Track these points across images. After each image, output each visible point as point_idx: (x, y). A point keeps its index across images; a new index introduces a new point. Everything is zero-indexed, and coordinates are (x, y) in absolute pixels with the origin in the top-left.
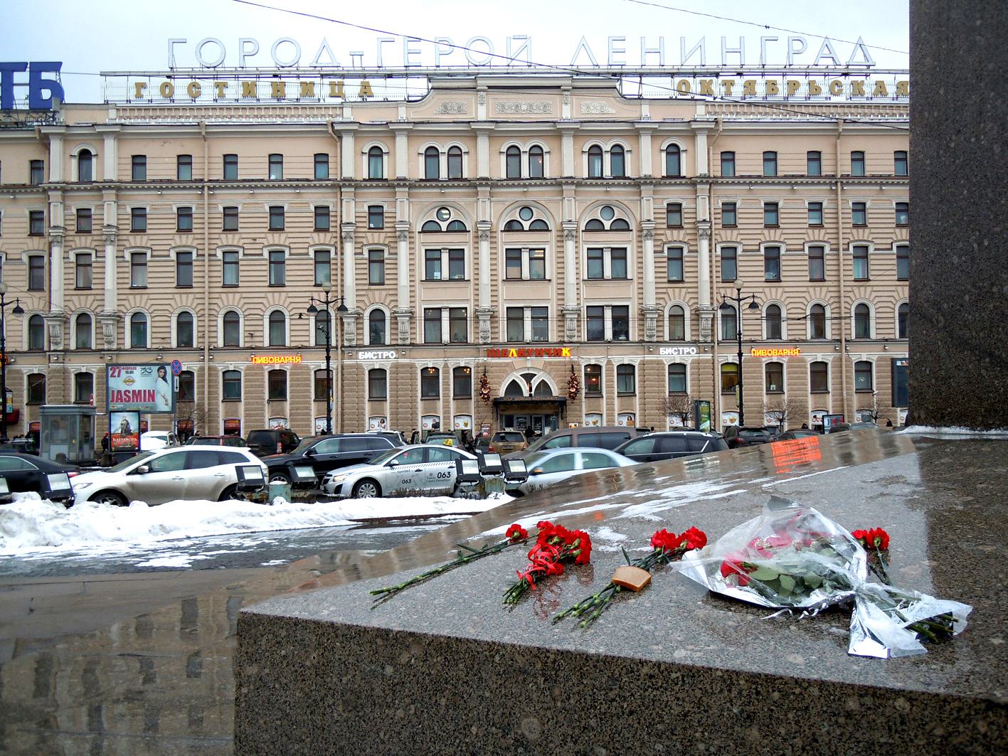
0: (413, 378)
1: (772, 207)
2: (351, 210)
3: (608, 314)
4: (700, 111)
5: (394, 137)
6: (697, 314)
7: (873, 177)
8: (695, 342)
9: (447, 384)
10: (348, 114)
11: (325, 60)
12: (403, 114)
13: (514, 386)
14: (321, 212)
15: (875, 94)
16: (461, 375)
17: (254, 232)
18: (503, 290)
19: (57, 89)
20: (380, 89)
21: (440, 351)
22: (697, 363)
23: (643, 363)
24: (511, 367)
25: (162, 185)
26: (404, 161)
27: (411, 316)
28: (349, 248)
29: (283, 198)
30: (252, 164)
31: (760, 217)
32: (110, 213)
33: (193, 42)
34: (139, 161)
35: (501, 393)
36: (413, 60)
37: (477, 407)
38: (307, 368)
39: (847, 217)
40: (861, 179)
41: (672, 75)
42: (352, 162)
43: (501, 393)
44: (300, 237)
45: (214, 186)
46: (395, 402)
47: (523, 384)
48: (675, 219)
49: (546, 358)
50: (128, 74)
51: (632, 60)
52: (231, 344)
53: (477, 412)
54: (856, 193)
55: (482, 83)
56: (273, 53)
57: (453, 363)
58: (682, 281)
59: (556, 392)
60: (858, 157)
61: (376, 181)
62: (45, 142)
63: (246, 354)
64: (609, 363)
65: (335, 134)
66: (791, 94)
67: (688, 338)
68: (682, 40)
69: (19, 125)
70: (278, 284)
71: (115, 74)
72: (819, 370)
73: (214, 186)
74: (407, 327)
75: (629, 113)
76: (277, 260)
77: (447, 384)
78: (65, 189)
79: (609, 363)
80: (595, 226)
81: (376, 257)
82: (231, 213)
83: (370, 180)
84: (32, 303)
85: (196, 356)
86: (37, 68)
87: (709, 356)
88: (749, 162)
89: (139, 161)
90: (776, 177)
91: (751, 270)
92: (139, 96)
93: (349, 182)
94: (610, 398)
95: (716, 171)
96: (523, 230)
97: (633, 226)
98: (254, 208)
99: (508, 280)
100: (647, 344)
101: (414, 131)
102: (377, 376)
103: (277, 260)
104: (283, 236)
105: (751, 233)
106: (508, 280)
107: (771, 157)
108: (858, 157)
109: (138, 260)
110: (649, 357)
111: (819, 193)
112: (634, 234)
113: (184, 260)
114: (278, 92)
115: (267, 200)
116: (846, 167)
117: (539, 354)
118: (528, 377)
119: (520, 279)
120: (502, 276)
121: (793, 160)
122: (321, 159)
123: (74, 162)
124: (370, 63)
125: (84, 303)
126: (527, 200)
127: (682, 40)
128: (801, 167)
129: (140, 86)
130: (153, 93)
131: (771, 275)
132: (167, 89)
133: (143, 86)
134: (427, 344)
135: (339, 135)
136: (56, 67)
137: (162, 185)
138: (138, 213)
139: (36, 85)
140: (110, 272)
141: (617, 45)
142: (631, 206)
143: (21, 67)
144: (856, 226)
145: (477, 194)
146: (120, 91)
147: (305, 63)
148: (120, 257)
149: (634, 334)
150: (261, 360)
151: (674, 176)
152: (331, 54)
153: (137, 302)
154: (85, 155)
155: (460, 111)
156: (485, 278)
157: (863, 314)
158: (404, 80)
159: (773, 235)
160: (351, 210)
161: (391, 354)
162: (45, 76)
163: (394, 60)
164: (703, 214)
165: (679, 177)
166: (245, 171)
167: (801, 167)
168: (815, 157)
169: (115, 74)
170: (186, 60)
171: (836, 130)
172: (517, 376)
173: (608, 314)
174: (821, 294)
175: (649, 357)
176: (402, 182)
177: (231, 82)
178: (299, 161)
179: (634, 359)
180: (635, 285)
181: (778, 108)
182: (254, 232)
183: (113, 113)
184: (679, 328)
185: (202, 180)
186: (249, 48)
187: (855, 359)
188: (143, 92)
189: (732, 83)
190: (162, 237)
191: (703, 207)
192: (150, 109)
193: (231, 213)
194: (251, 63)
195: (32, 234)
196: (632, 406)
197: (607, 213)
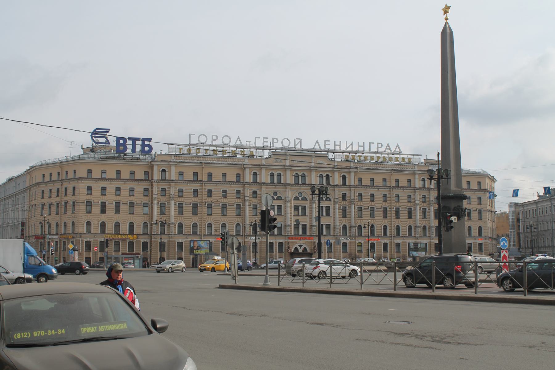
1: (372, 195)
2: (248, 192)
4: (352, 165)
5: (170, 167)
6: (350, 227)
7: (186, 181)
8: (350, 236)
9: (276, 248)
11: (238, 143)
13: (296, 249)
15: (402, 161)
16: (281, 244)
19: (151, 148)
21: (273, 237)
24: (296, 243)
26: (265, 177)
29: (182, 186)
31: (406, 199)
32: (173, 190)
35: (292, 251)
36: (266, 144)
37: (285, 255)
39: (394, 199)
40: (397, 187)
43: (292, 251)
44: (232, 199)
46: (169, 251)
47: (299, 248)
48: (163, 193)
49: (306, 240)
51: (331, 147)
52: (180, 232)
53: (285, 257)
54: (209, 187)
57: (278, 241)
58: (134, 214)
59: (309, 251)
60: (397, 181)
63: (93, 236)
65: (243, 168)
66: (378, 160)
67: (348, 235)
69: (138, 159)
72: (385, 245)
76: (224, 207)
77: (276, 248)
80: (296, 199)
82: (210, 192)
83: (162, 180)
86: (144, 140)
87: (354, 240)
88: (366, 181)
90: (226, 181)
91: (366, 214)
94: (276, 253)
95: (357, 183)
96: (299, 200)
97: (332, 199)
103: (224, 207)
104: (106, 197)
105: (379, 203)
107: (224, 175)
108: (397, 181)
109: (360, 209)
111: (385, 191)
112: (332, 202)
113: (195, 206)
114: (189, 150)
115: (222, 187)
116: (393, 184)
117: (304, 239)
118: (300, 246)
120: (293, 214)
121: (378, 181)
122: (238, 175)
124: (252, 144)
125: (345, 222)
126: (300, 191)
128: (406, 184)
129: (181, 149)
131: (238, 213)
132: (189, 150)
133: (182, 149)
134: (143, 234)
135: (245, 168)
136: (150, 140)
139: (143, 145)
143: (138, 139)
144: (396, 202)
145: (286, 188)
149: (308, 233)
156: (289, 215)
157: (398, 228)
159: (373, 204)
162: (146, 143)
163: (259, 144)
164: (173, 192)
165: (305, 184)
167: (220, 178)
168: (385, 180)
170: (194, 141)
172: (297, 246)
174: (386, 222)
179: (92, 240)
181: (406, 168)
183: (173, 158)
184: (146, 230)
185: (201, 181)
187: (396, 242)
188: (182, 151)
189: (361, 156)
190: (188, 198)
191: (353, 195)
197: (300, 195)
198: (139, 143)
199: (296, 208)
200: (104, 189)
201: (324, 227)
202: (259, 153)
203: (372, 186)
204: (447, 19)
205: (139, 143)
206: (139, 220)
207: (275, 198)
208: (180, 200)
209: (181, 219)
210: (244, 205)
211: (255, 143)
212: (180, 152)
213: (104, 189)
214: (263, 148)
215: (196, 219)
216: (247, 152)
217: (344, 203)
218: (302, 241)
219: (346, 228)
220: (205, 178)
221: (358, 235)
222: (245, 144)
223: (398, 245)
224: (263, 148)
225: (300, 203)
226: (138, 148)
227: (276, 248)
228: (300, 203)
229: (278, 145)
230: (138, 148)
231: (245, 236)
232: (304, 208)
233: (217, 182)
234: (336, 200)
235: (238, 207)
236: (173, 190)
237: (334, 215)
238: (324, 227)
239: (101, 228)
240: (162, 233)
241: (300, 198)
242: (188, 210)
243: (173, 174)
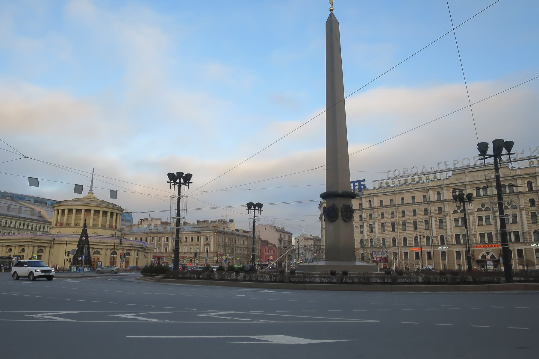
0: (454, 254)
3: (486, 235)
5: (536, 178)
10: (431, 184)
11: (424, 171)
12: (445, 182)
14: (426, 210)
17: (409, 218)
18: (478, 228)
19: (364, 185)
20: (439, 176)
21: (460, 246)
22: (448, 251)
23: (525, 249)
24: (481, 251)
25: (387, 206)
26: (447, 195)
27: (451, 236)
28: (433, 219)
29: (383, 210)
30: (408, 199)
32: (376, 215)
33: (392, 171)
34: (382, 202)
35: (480, 258)
36: (448, 167)
38: (453, 250)
41: (529, 159)
42: (432, 196)
43: (480, 258)
44: (421, 217)
45: (399, 205)
46: (448, 260)
50: (378, 181)
52: (405, 245)
54: (402, 208)
55: (466, 171)
56: (462, 163)
61: (439, 200)
62: (361, 199)
63: (409, 248)
64: (514, 249)
68: (530, 148)
70: (405, 230)
71: (376, 181)
73: (399, 205)
74: (528, 237)
75: (513, 173)
78: (366, 209)
79: (514, 249)
80: (479, 210)
81: (441, 221)
84: (427, 233)
85: (397, 248)
86: (360, 181)
89: (382, 202)
92: (381, 185)
93: (431, 202)
98: (409, 210)
99: (479, 225)
100: (526, 243)
101: (448, 186)
102: (443, 253)
105: (388, 219)
106: (479, 225)
110: (527, 247)
113: (393, 225)
114: (413, 180)
115: (412, 208)
119: (483, 225)
122: (424, 197)
123: (368, 203)
124: (436, 169)
125: (442, 232)
126: (483, 202)
127: (530, 148)
128: (389, 203)
130: (384, 185)
135: (428, 190)
136: (364, 181)
137: (387, 206)
138: (382, 214)
140: (377, 229)
141: (447, 163)
142: (516, 201)
143: (356, 182)
146: (377, 185)
147: (419, 172)
148: (527, 214)
150: (413, 249)
151: (439, 200)
152: (426, 169)
153: (383, 235)
154: (370, 201)
155: (461, 179)
158: (181, 212)
160: (433, 209)
161: (447, 247)
162: (362, 183)
163: (442, 168)
166: (385, 204)
167: (389, 203)
169: (376, 181)
170: (391, 175)
171: (394, 193)
172: (484, 253)
173: (486, 235)
174: (394, 235)
175: (527, 247)
176: (446, 200)
177: (401, 179)
178: (419, 198)
179: (523, 248)
180: (520, 224)
182: (409, 218)
186: (456, 162)
190: (388, 219)
192: (384, 188)
193: (403, 212)
194: (406, 174)
195: (425, 215)
196: (445, 263)
198: (357, 184)
199: (480, 219)
200: (414, 212)
201: (512, 234)
202: (439, 176)
203: (403, 204)
204: (331, 10)
205: (357, 184)
206: (411, 234)
207: (483, 209)
208: (383, 220)
209: (383, 235)
210: (374, 224)
211: (439, 167)
212: (381, 185)
213: (414, 212)
214: (446, 171)
215: (394, 235)
216: (431, 177)
217: (441, 216)
218: (488, 249)
219: (444, 238)
220: (400, 202)
221: (489, 241)
222: (430, 170)
223: (406, 254)
224: (446, 171)
225: (483, 214)
226: (357, 187)
227: (463, 255)
228: (483, 214)
229: (460, 165)
230: (357, 187)
231: (526, 243)
232: (487, 218)
233: (408, 204)
234: (521, 207)
235: (427, 222)
236: (376, 215)
237: (522, 221)
238: (512, 234)
239: (415, 242)
240: (428, 245)
241: (483, 209)
242: (388, 228)
243: (376, 202)
